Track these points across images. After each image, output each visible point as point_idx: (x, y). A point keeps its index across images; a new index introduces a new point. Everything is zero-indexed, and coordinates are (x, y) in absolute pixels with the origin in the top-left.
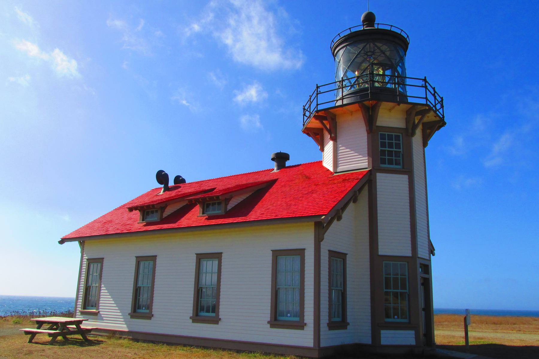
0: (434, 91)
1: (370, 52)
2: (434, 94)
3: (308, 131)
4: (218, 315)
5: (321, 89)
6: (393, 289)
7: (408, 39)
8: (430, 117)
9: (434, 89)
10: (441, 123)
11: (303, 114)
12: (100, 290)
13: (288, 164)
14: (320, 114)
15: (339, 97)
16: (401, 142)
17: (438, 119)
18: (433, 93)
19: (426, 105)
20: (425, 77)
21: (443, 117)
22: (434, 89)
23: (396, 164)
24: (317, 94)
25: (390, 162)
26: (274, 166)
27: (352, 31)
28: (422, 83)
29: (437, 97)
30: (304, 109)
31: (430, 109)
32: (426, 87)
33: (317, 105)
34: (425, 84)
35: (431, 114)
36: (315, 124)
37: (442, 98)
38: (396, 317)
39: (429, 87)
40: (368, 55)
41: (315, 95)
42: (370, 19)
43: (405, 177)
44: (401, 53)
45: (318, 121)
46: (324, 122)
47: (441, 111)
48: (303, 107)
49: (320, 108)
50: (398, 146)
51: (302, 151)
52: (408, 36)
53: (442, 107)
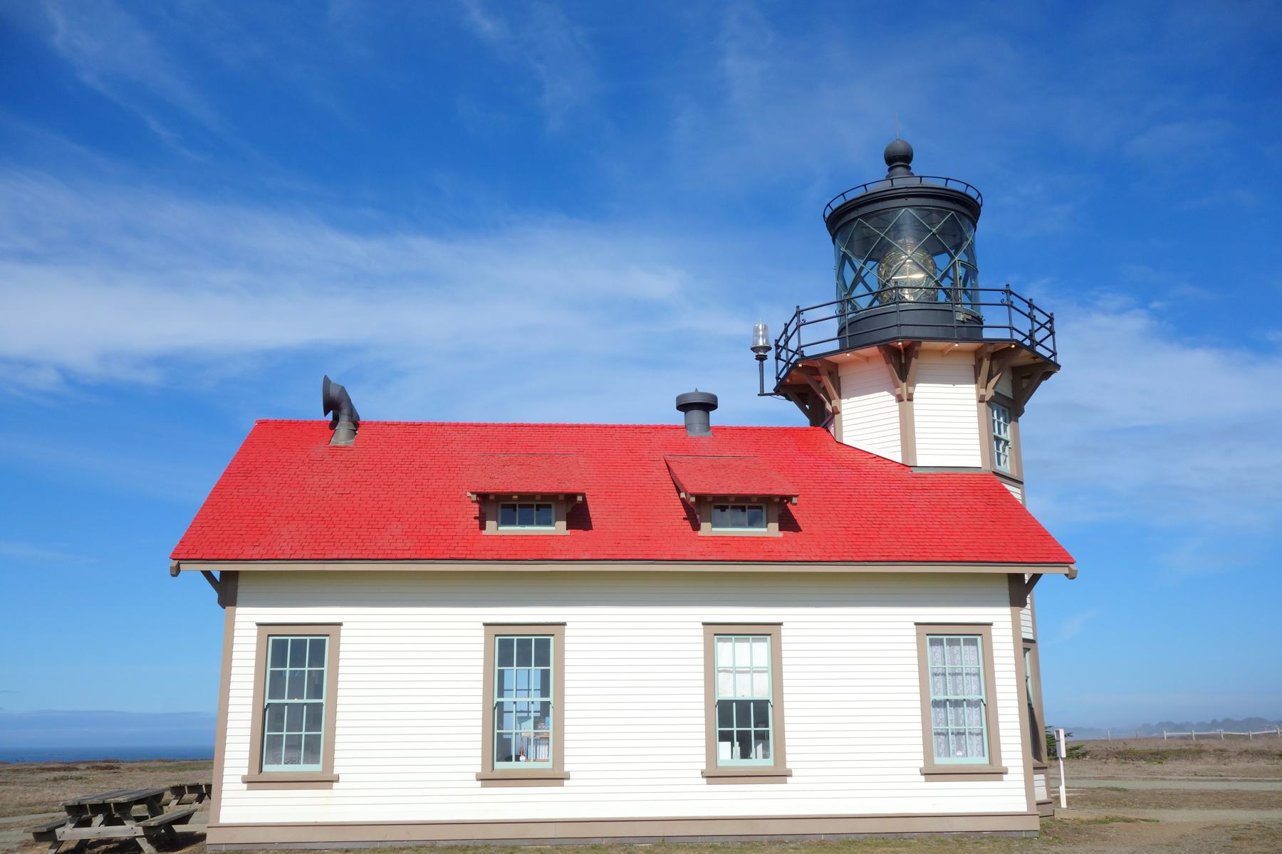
0: (1031, 306)
4: (330, 764)
5: (807, 316)
8: (1023, 358)
9: (1031, 306)
10: (1046, 368)
21: (1054, 354)
24: (798, 327)
31: (1020, 345)
32: (1011, 306)
35: (1024, 352)
39: (1018, 303)
53: (1052, 333)
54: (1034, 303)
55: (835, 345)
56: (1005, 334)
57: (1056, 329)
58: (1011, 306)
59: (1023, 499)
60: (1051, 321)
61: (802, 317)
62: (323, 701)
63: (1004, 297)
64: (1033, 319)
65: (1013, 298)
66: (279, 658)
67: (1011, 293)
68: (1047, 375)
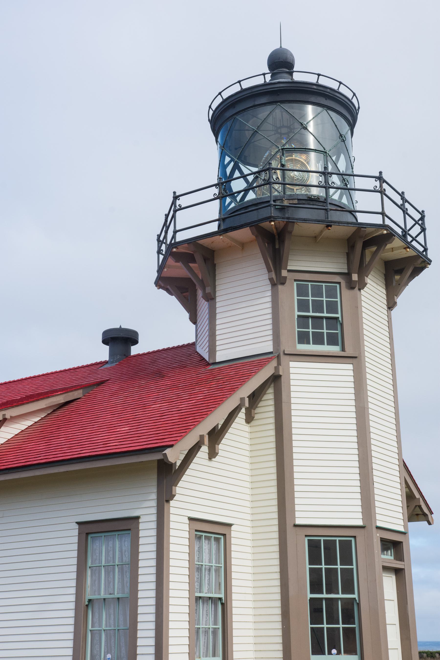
0: (403, 198)
1: (283, 126)
2: (403, 205)
3: (163, 282)
5: (183, 202)
6: (327, 593)
7: (354, 101)
9: (402, 195)
10: (417, 263)
11: (156, 249)
12: (135, 646)
13: (135, 350)
14: (181, 249)
15: (201, 218)
16: (296, 298)
17: (410, 253)
18: (400, 202)
19: (384, 226)
20: (381, 173)
21: (426, 250)
22: (402, 195)
23: (315, 342)
24: (175, 211)
25: (318, 340)
26: (103, 353)
27: (244, 87)
28: (372, 184)
29: (411, 211)
30: (158, 240)
31: (391, 235)
32: (382, 192)
33: (175, 232)
34: (381, 186)
36: (178, 270)
37: (422, 214)
38: (334, 651)
39: (389, 191)
40: (281, 134)
41: (172, 213)
42: (280, 62)
43: (346, 370)
44: (345, 128)
45: (180, 264)
46: (191, 265)
47: (421, 239)
48: (156, 237)
49: (180, 237)
50: (332, 307)
51: (164, 325)
52: (354, 94)
53: (423, 230)
54: (406, 196)
55: (214, 227)
56: (377, 220)
57: (427, 225)
58: (382, 192)
59: (348, 130)
60: (422, 218)
61: (178, 202)
62: (310, 626)
63: (378, 183)
64: (405, 212)
65: (385, 186)
66: (350, 634)
67: (385, 181)
68: (417, 271)
